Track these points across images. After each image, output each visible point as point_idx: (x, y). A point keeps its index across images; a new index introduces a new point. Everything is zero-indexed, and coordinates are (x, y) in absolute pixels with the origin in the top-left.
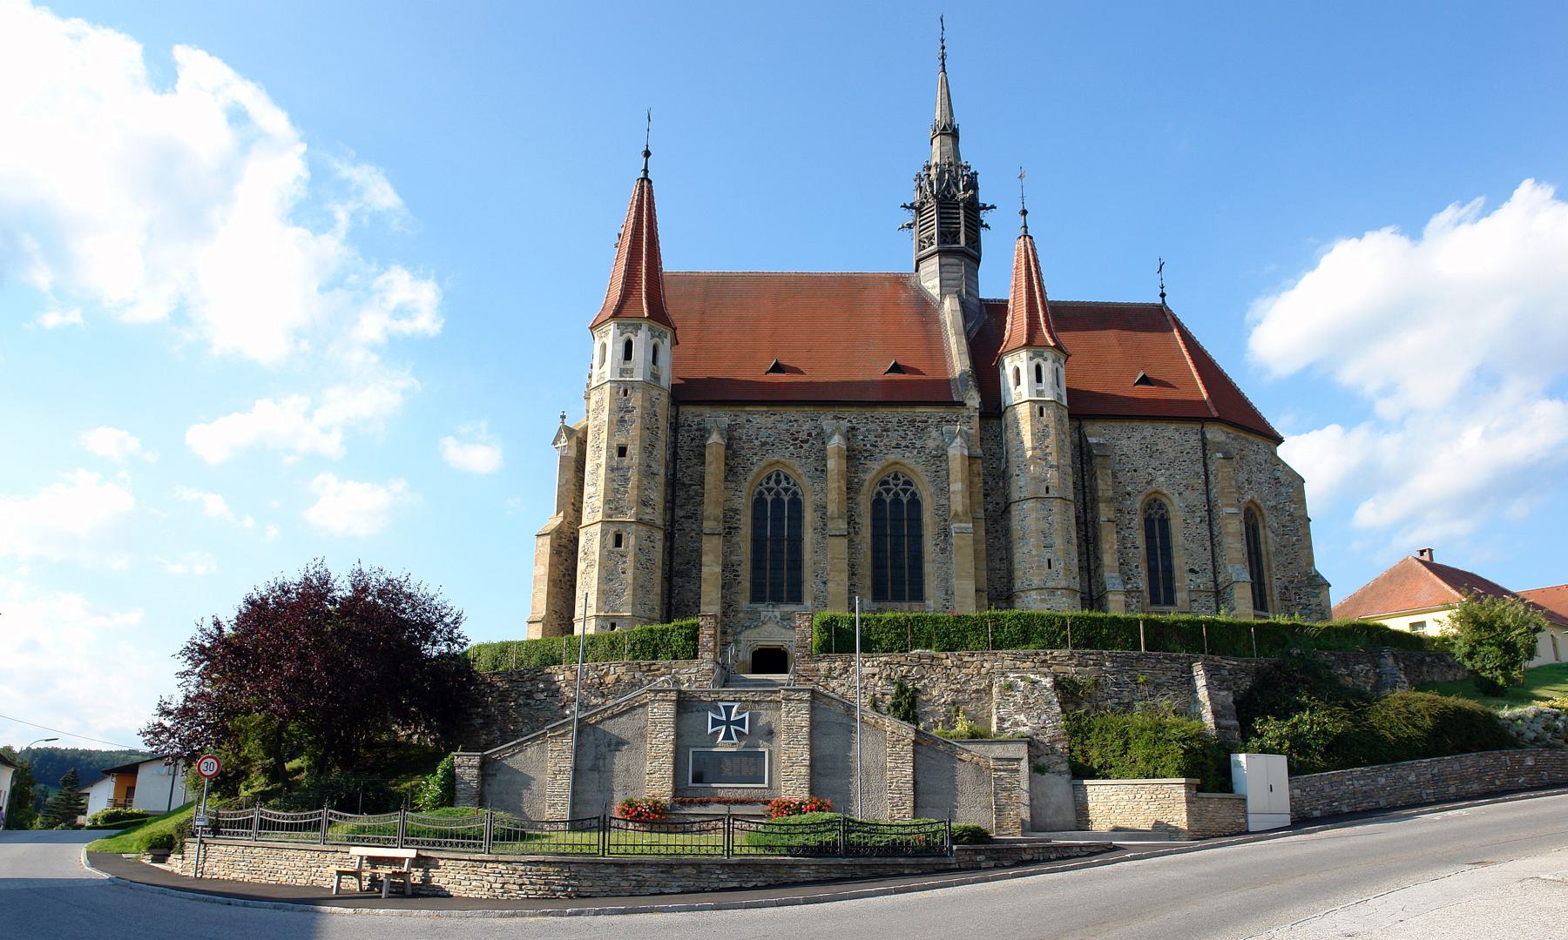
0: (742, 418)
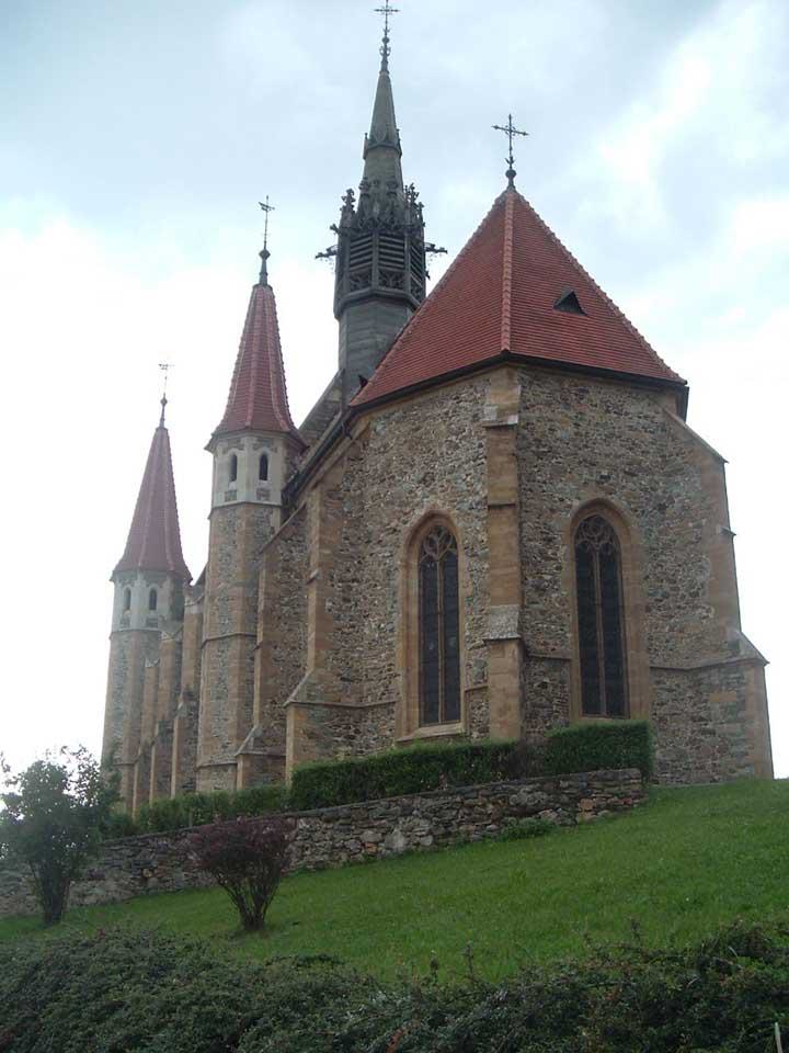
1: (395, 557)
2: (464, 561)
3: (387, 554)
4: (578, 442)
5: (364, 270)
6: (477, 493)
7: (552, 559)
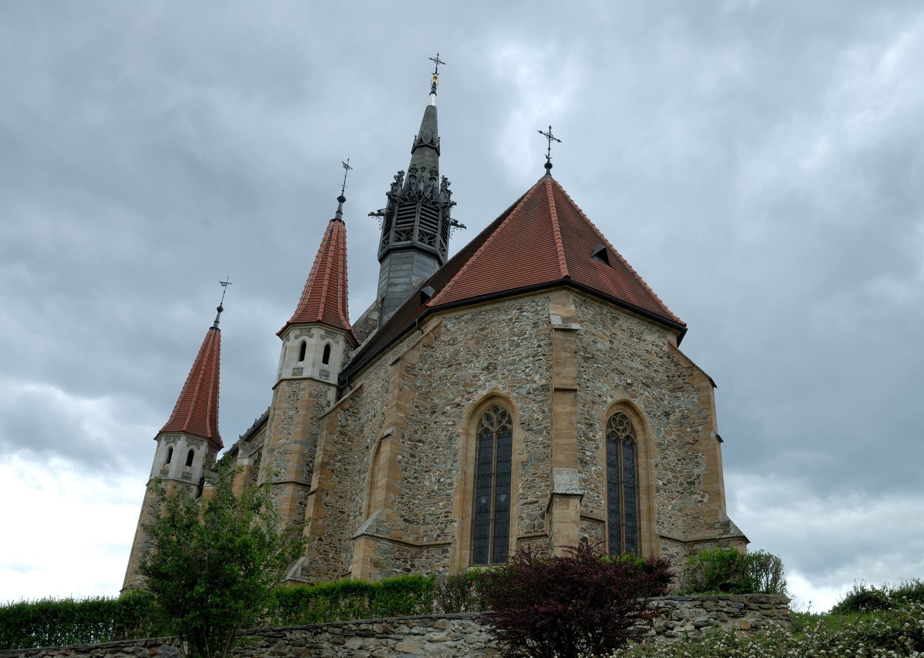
1: (458, 426)
2: (518, 434)
3: (450, 423)
4: (612, 354)
5: (407, 228)
6: (535, 382)
7: (592, 440)
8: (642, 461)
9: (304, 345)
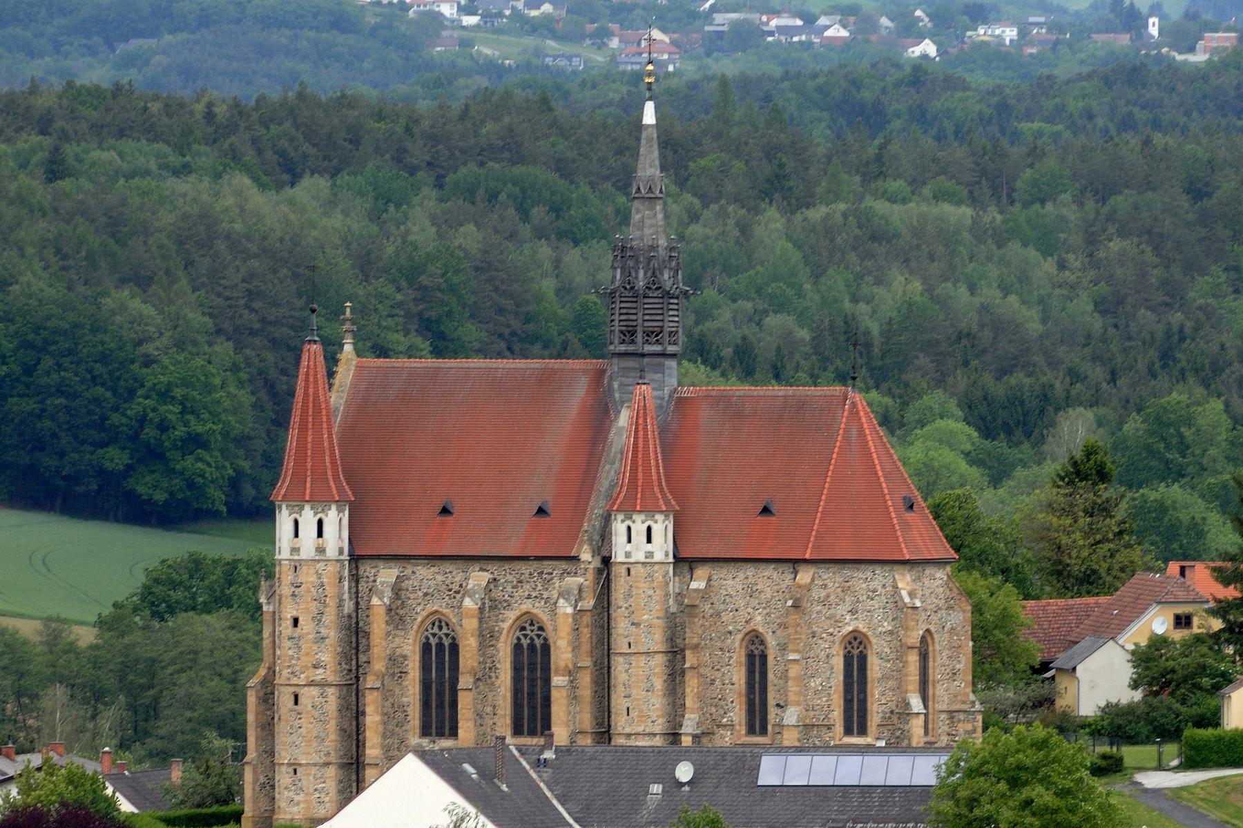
0: (408, 571)
8: (931, 664)
9: (649, 529)
